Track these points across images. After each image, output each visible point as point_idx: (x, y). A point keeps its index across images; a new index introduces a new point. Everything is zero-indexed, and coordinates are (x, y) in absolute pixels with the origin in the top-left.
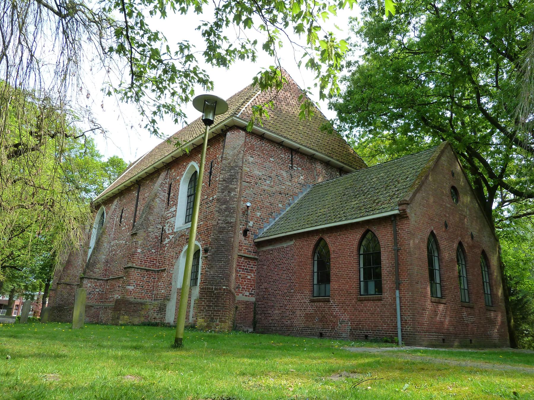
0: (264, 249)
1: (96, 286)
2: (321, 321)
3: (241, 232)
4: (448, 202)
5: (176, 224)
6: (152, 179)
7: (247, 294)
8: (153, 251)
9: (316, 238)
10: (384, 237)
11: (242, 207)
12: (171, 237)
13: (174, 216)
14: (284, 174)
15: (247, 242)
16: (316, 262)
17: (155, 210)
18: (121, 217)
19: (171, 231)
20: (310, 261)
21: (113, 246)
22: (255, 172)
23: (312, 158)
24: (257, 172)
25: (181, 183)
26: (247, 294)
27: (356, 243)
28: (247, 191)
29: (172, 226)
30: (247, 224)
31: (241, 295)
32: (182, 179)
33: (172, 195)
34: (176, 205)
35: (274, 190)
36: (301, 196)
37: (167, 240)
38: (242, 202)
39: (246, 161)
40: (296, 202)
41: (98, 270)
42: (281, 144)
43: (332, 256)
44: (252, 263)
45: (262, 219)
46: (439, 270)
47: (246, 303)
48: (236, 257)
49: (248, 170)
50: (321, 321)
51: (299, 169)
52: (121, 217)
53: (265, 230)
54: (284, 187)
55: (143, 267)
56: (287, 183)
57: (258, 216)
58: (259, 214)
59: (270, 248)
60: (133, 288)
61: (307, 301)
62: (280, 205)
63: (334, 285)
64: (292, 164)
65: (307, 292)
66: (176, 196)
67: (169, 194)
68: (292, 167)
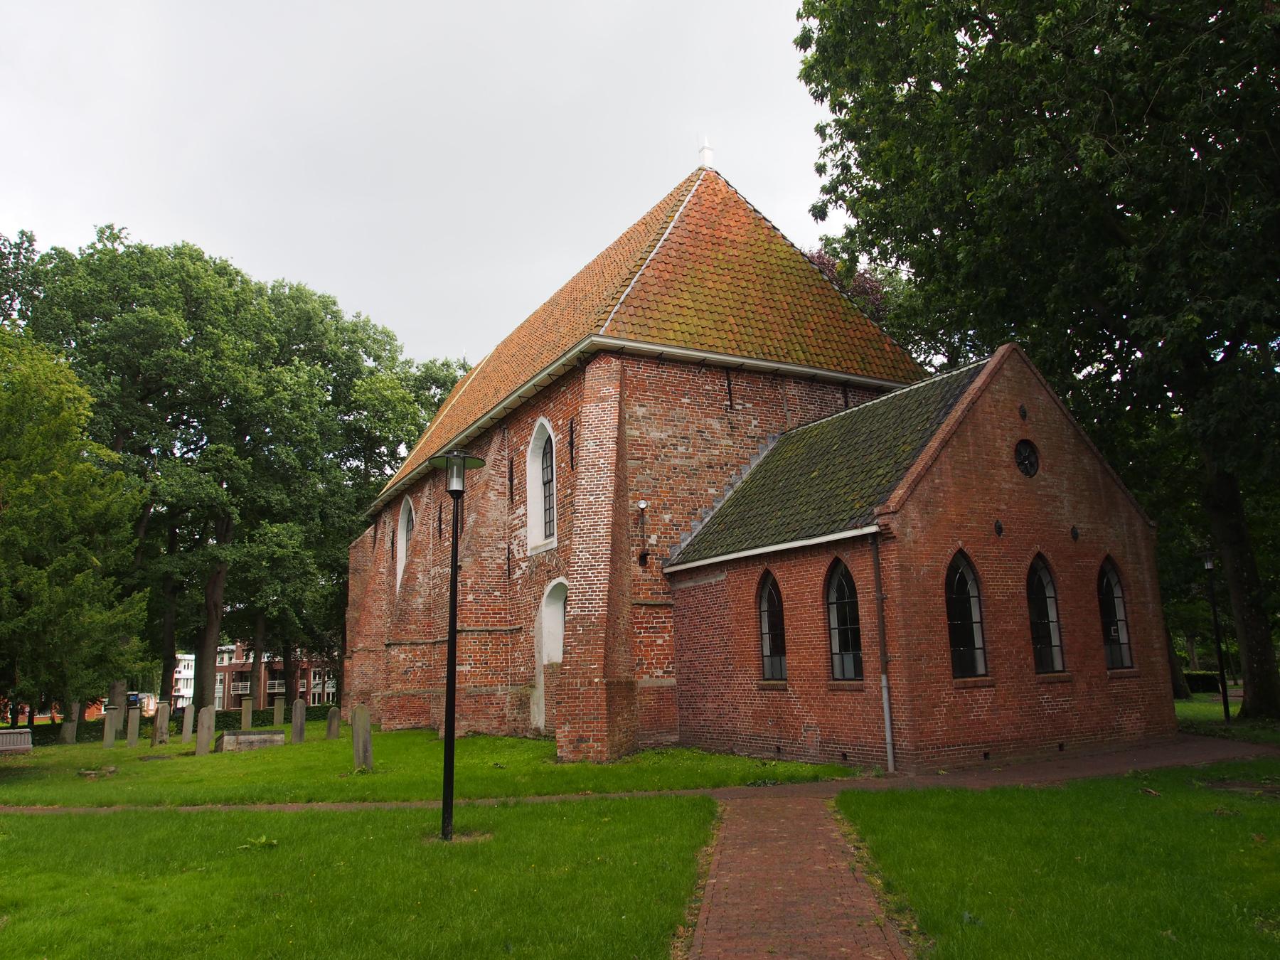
0: (682, 586)
1: (414, 656)
2: (777, 725)
3: (635, 559)
4: (1008, 478)
5: (529, 541)
6: (480, 448)
7: (660, 673)
8: (497, 593)
9: (759, 570)
10: (861, 569)
11: (631, 510)
12: (524, 565)
13: (524, 525)
14: (716, 425)
15: (648, 576)
16: (765, 616)
17: (489, 514)
18: (440, 520)
19: (522, 555)
20: (753, 613)
21: (434, 578)
22: (652, 435)
23: (777, 377)
24: (655, 435)
25: (528, 459)
26: (660, 673)
27: (820, 581)
28: (640, 477)
29: (523, 545)
30: (644, 542)
31: (646, 677)
32: (529, 450)
33: (516, 481)
34: (524, 502)
35: (694, 462)
36: (755, 463)
37: (518, 573)
38: (631, 502)
39: (631, 417)
40: (745, 477)
41: (414, 627)
42: (701, 364)
43: (786, 605)
44: (662, 614)
45: (674, 525)
46: (981, 622)
47: (659, 691)
48: (627, 608)
49: (637, 433)
50: (777, 725)
51: (748, 405)
52: (440, 520)
53: (684, 545)
54: (717, 452)
55: (483, 628)
56: (724, 442)
57: (667, 521)
58: (667, 517)
59: (691, 584)
60: (468, 668)
61: (754, 687)
62: (712, 491)
63: (791, 660)
64: (730, 400)
65: (753, 671)
66: (523, 483)
67: (511, 480)
68: (731, 406)
